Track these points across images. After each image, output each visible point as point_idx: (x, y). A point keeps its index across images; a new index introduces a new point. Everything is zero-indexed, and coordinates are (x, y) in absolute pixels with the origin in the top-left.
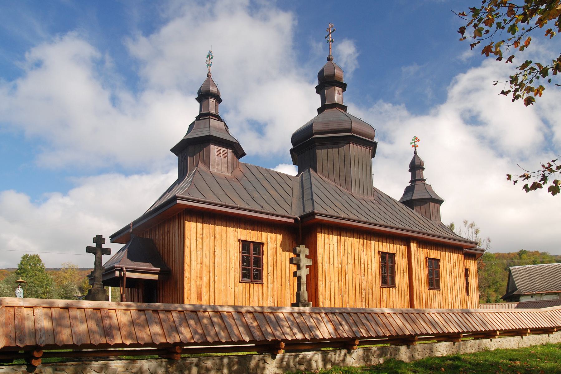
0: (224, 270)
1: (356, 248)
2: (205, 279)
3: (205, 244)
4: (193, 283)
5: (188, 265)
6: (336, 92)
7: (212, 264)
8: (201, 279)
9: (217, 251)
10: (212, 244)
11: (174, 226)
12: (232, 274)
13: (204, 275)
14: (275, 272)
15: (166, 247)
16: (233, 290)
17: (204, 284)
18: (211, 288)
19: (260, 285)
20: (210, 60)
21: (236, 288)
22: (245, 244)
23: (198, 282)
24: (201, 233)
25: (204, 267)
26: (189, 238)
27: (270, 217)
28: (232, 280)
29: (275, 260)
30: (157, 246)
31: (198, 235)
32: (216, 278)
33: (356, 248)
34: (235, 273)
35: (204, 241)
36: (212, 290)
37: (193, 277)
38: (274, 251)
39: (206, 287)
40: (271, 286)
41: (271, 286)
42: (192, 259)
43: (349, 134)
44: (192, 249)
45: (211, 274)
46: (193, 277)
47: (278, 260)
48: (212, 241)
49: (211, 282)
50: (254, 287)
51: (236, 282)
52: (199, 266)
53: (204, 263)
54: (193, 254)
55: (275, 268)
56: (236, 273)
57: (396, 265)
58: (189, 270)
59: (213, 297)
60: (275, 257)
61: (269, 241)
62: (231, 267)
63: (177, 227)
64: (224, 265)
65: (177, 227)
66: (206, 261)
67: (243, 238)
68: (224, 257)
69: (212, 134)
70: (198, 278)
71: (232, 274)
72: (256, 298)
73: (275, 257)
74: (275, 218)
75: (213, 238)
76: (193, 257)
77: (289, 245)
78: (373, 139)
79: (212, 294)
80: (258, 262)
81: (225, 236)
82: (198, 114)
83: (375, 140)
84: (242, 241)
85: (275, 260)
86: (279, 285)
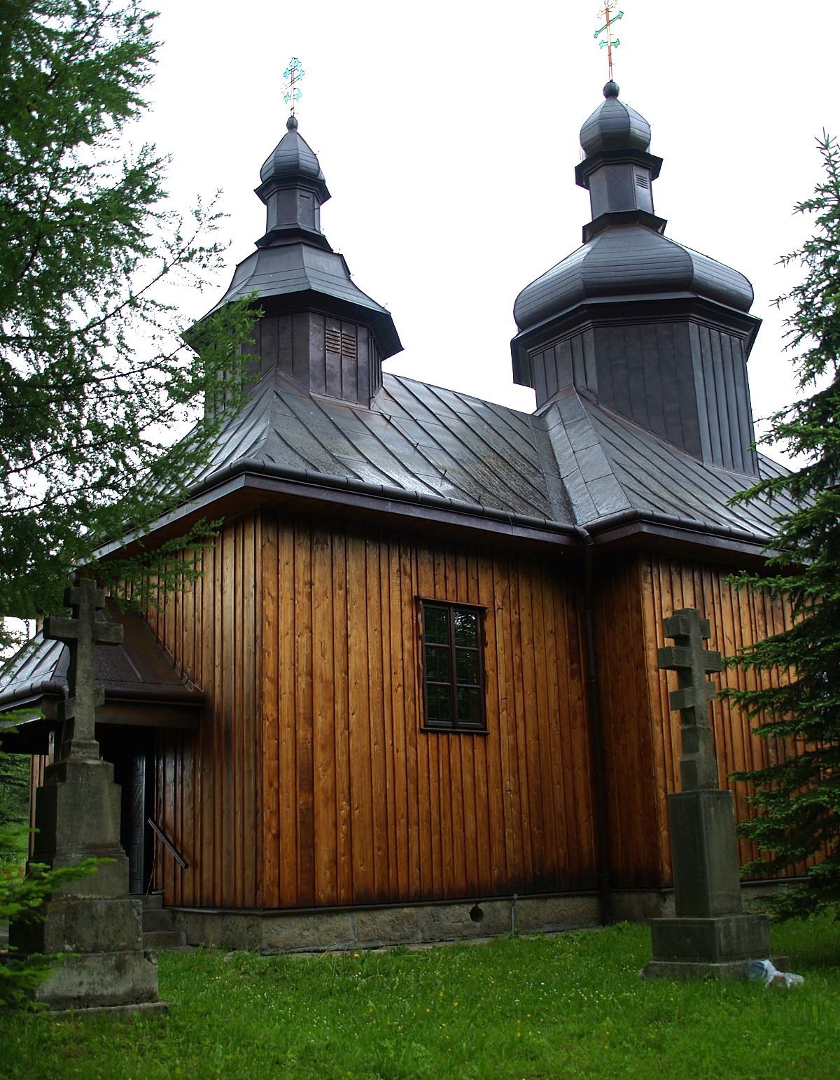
0: (375, 692)
1: (745, 620)
2: (320, 721)
3: (318, 614)
4: (286, 734)
5: (271, 680)
6: (635, 177)
7: (339, 676)
8: (311, 721)
9: (353, 633)
10: (339, 614)
11: (218, 560)
12: (398, 705)
13: (317, 711)
14: (519, 696)
15: (189, 624)
16: (401, 756)
17: (319, 738)
18: (339, 752)
19: (478, 740)
20: (293, 82)
21: (411, 749)
22: (432, 613)
23: (301, 733)
24: (307, 578)
25: (318, 687)
26: (274, 594)
27: (491, 527)
28: (399, 723)
29: (517, 659)
30: (153, 622)
31: (300, 586)
32: (353, 718)
33: (745, 620)
34: (405, 707)
35: (315, 605)
36: (341, 758)
37: (286, 716)
38: (515, 632)
39: (323, 748)
40: (507, 740)
41: (507, 740)
42: (282, 660)
43: (687, 295)
44: (281, 627)
45: (339, 707)
46: (286, 716)
47: (526, 660)
48: (339, 604)
49: (338, 732)
50: (462, 748)
51: (409, 729)
52: (303, 682)
53: (317, 672)
54: (286, 643)
55: (518, 685)
56: (409, 702)
57: (488, 651)
58: (273, 694)
59: (345, 778)
60: (516, 651)
61: (498, 602)
62: (395, 684)
63: (229, 562)
64: (375, 676)
65: (229, 562)
66: (322, 665)
67: (426, 593)
68: (373, 654)
69: (315, 287)
70: (302, 723)
71: (398, 705)
72: (468, 779)
73: (516, 651)
74: (518, 532)
75: (341, 593)
76: (285, 654)
77: (555, 614)
78: (747, 310)
79: (342, 769)
80: (474, 670)
81: (376, 589)
82: (262, 233)
83: (754, 312)
84: (425, 601)
85: (517, 659)
86: (530, 738)
